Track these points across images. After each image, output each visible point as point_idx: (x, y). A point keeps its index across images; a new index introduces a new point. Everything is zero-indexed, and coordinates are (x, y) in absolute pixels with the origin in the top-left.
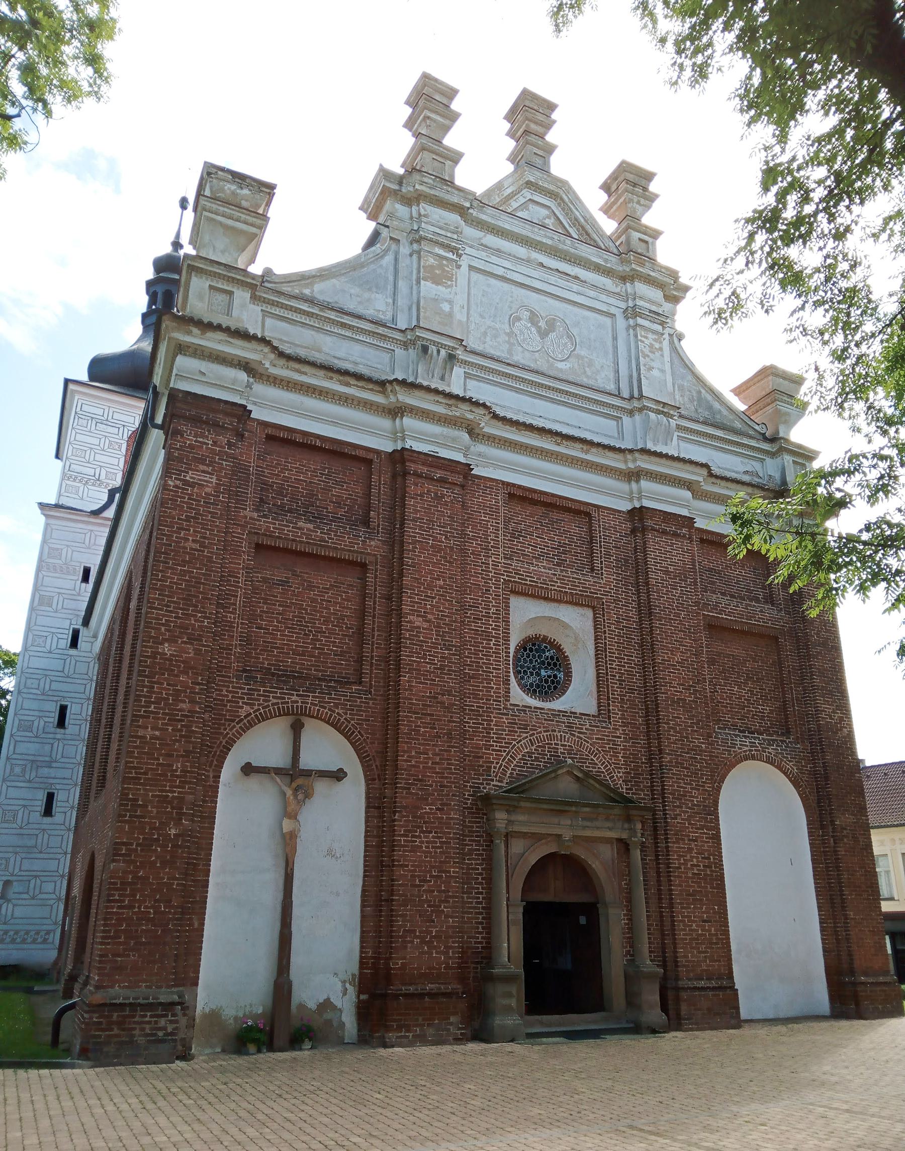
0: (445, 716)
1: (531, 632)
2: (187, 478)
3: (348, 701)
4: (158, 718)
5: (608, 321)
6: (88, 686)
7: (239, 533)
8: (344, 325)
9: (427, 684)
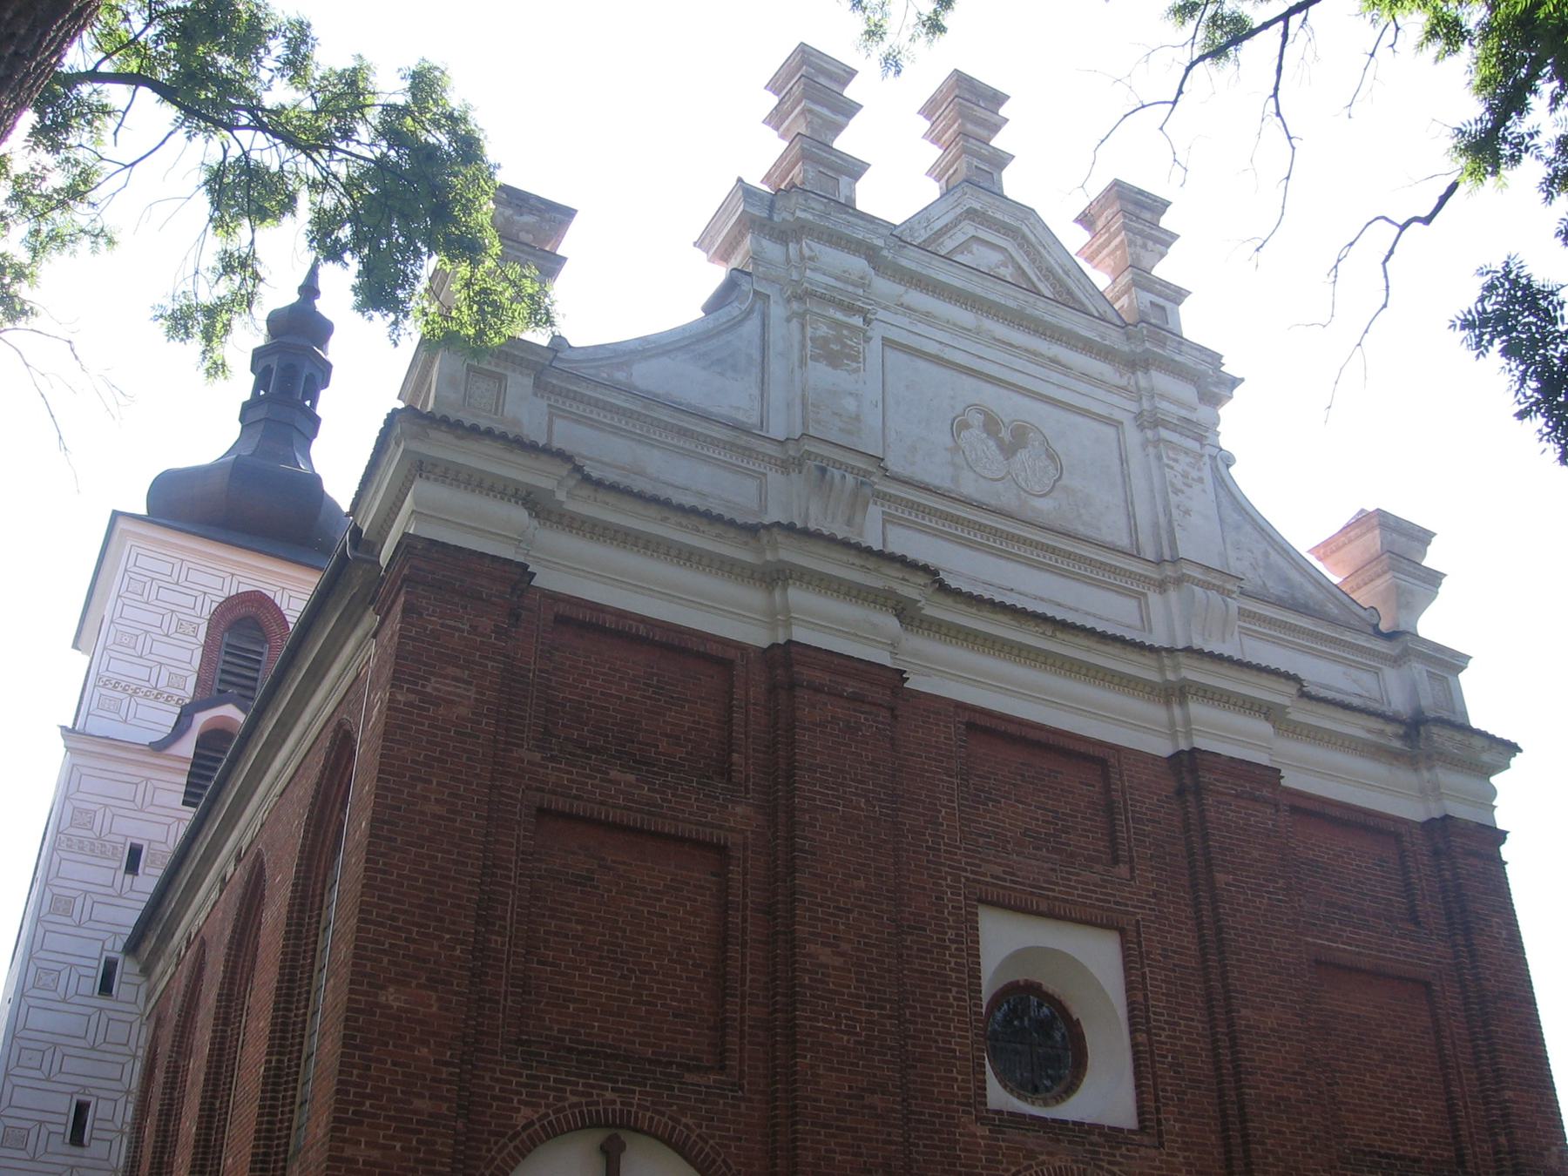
0: (877, 1132)
1: (1020, 976)
2: (429, 690)
3: (703, 1102)
5: (1110, 432)
6: (128, 1069)
7: (509, 789)
8: (683, 433)
9: (843, 1071)
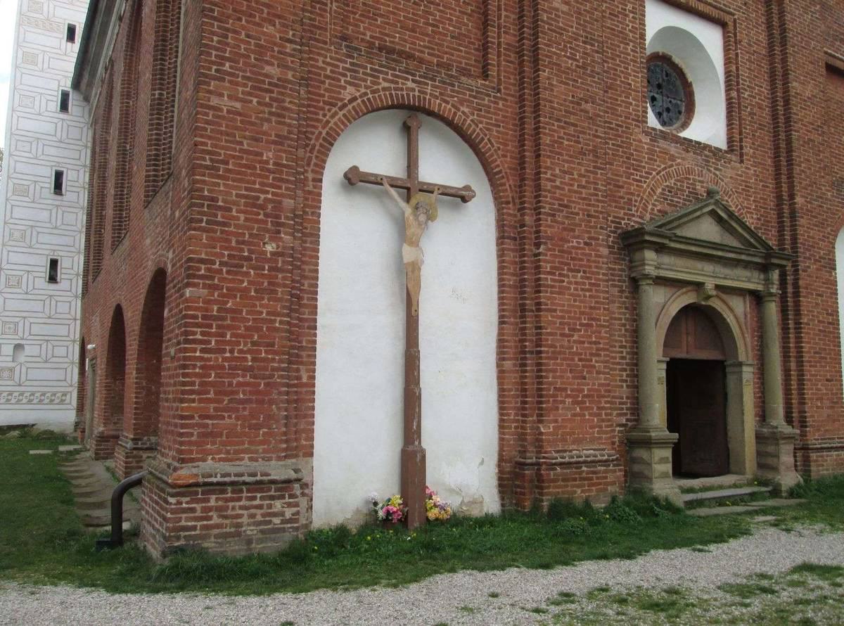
0: (590, 129)
4: (237, 84)
